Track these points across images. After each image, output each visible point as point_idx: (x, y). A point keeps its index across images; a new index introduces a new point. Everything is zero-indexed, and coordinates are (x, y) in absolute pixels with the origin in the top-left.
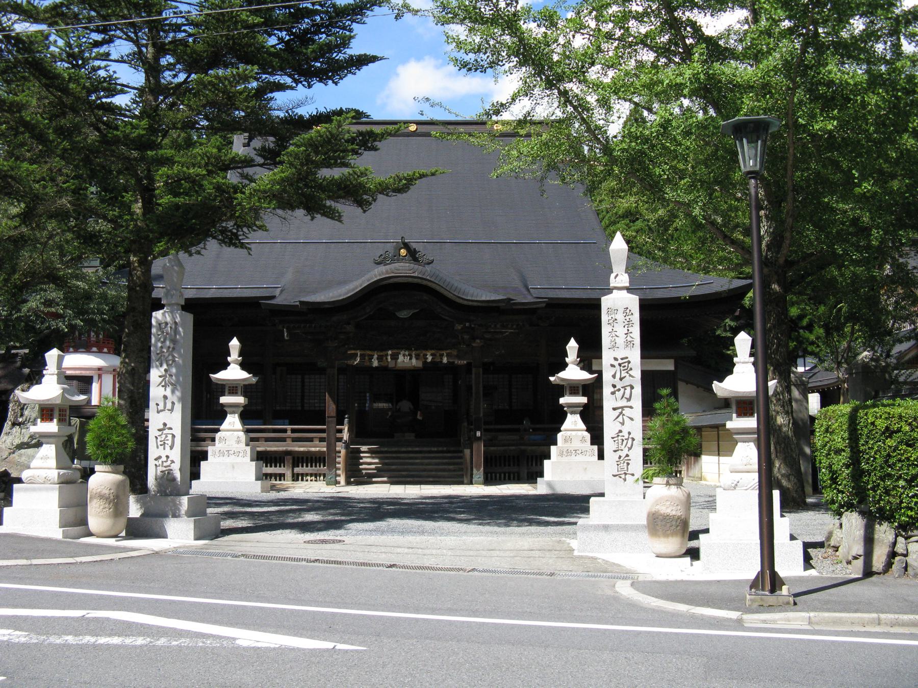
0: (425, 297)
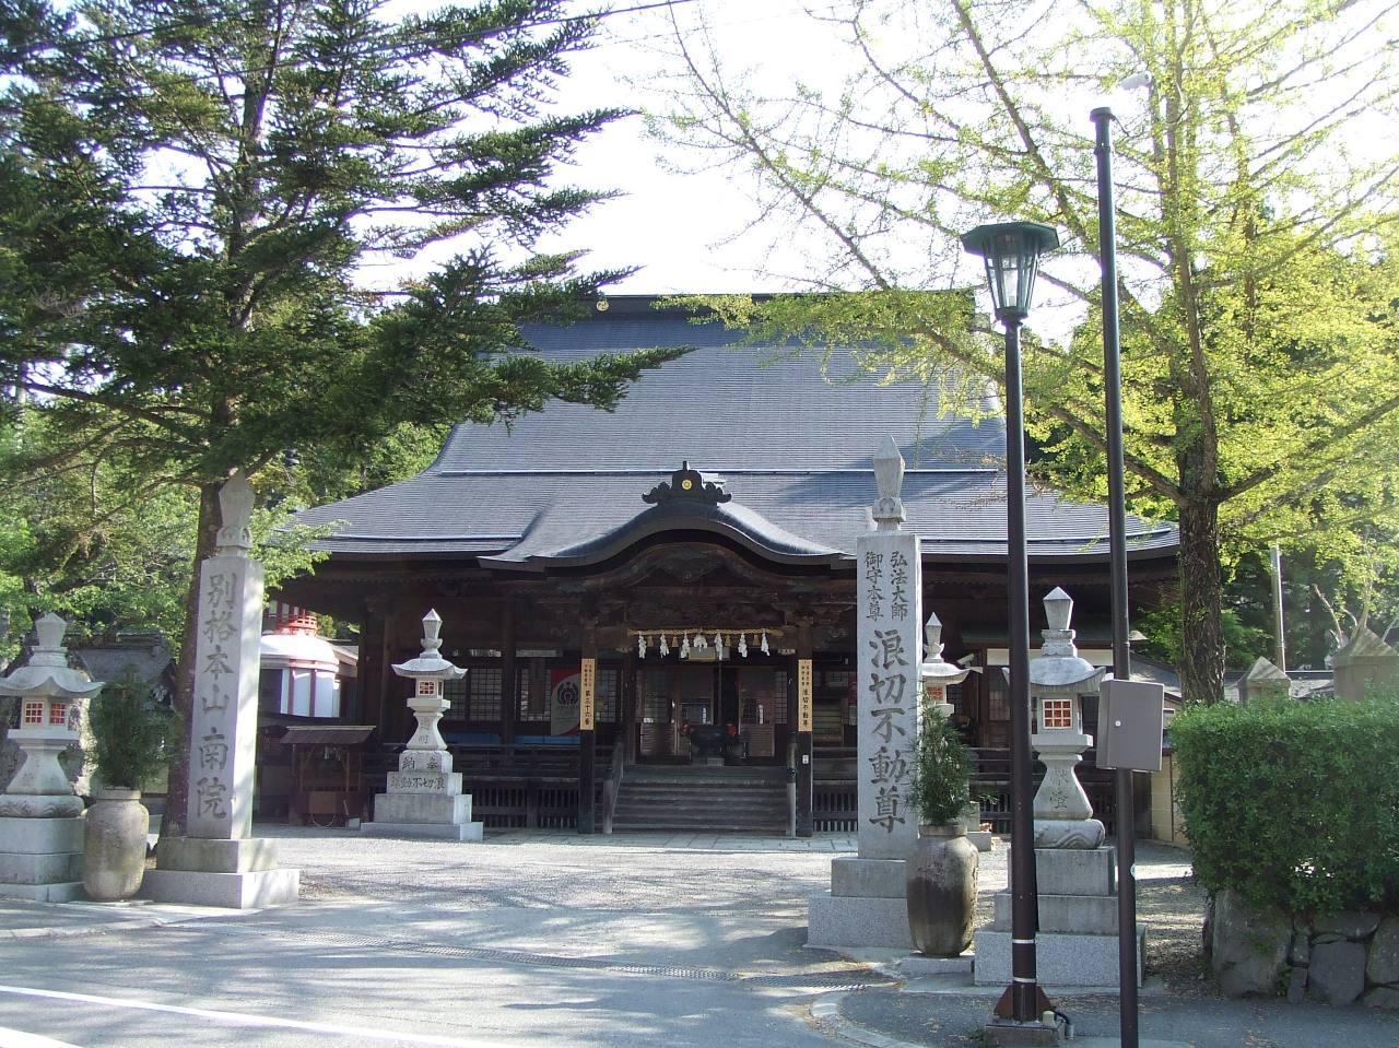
0: (721, 551)
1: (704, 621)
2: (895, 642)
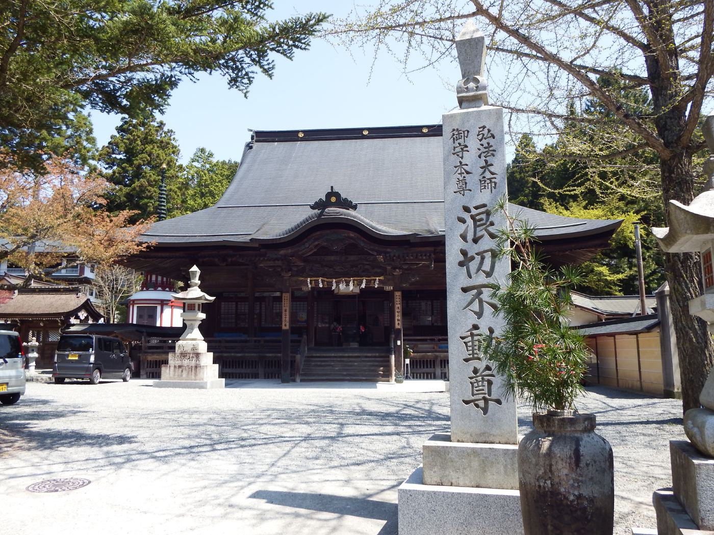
0: (352, 234)
1: (344, 275)
2: (484, 216)
